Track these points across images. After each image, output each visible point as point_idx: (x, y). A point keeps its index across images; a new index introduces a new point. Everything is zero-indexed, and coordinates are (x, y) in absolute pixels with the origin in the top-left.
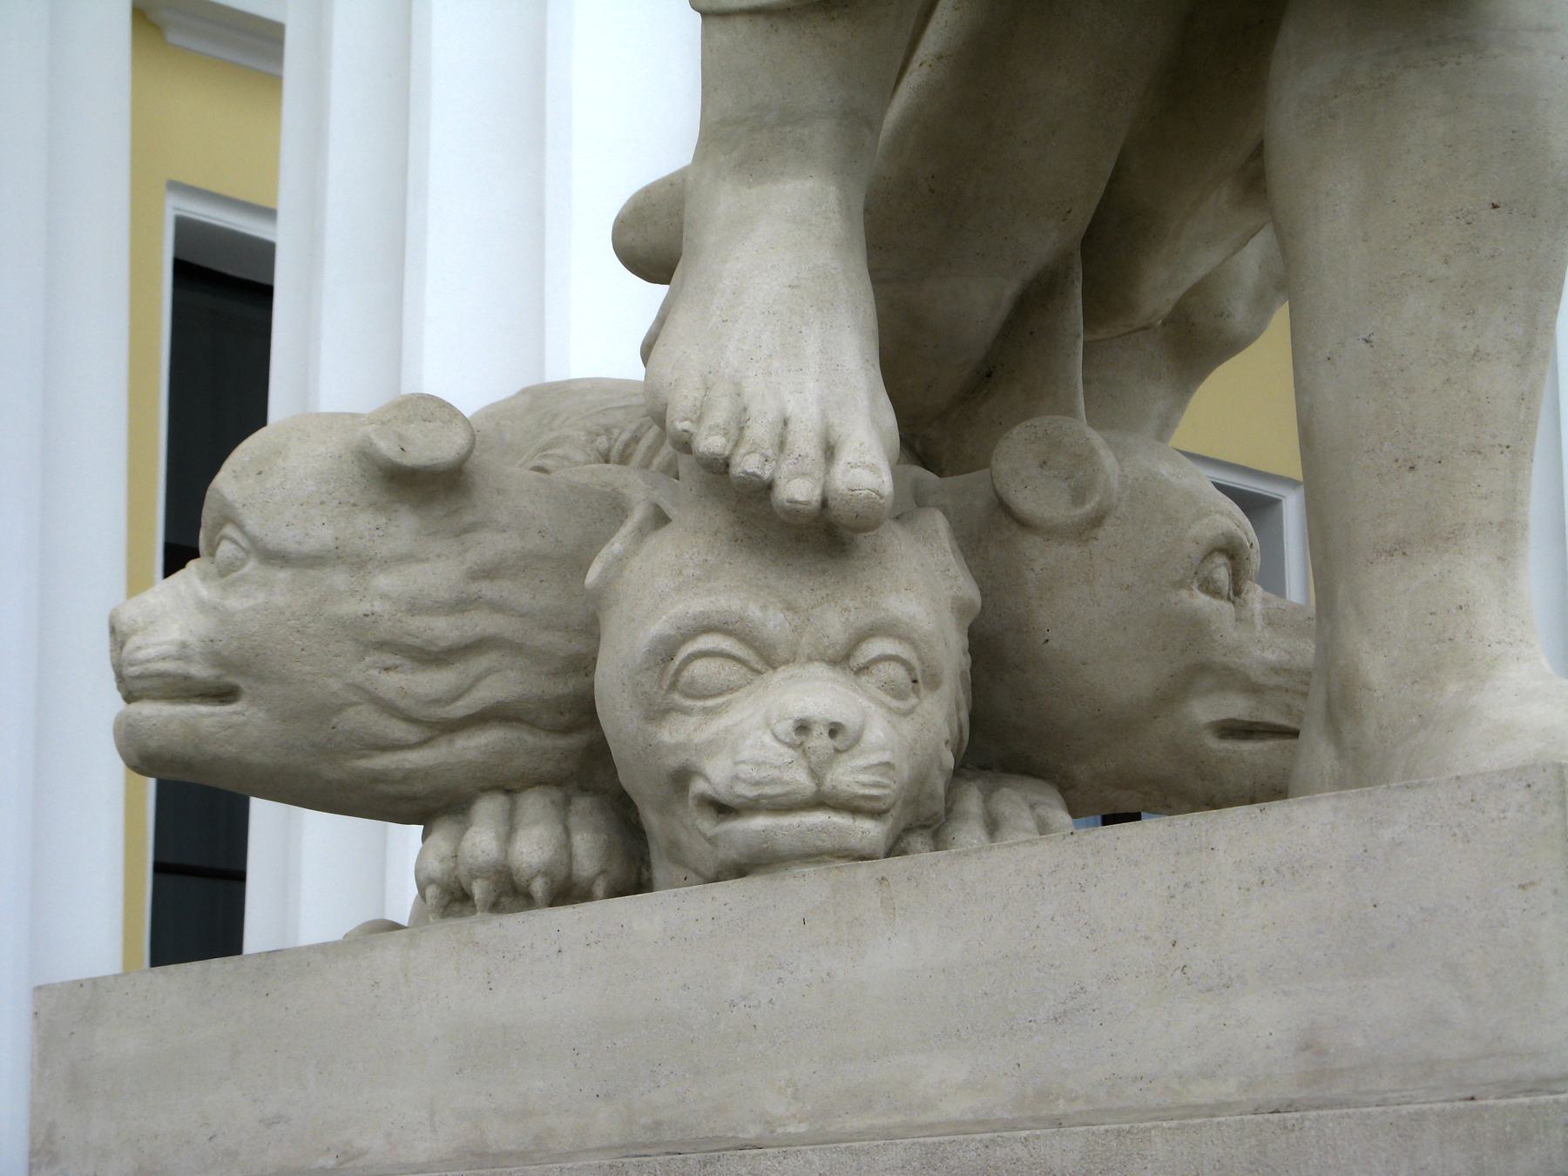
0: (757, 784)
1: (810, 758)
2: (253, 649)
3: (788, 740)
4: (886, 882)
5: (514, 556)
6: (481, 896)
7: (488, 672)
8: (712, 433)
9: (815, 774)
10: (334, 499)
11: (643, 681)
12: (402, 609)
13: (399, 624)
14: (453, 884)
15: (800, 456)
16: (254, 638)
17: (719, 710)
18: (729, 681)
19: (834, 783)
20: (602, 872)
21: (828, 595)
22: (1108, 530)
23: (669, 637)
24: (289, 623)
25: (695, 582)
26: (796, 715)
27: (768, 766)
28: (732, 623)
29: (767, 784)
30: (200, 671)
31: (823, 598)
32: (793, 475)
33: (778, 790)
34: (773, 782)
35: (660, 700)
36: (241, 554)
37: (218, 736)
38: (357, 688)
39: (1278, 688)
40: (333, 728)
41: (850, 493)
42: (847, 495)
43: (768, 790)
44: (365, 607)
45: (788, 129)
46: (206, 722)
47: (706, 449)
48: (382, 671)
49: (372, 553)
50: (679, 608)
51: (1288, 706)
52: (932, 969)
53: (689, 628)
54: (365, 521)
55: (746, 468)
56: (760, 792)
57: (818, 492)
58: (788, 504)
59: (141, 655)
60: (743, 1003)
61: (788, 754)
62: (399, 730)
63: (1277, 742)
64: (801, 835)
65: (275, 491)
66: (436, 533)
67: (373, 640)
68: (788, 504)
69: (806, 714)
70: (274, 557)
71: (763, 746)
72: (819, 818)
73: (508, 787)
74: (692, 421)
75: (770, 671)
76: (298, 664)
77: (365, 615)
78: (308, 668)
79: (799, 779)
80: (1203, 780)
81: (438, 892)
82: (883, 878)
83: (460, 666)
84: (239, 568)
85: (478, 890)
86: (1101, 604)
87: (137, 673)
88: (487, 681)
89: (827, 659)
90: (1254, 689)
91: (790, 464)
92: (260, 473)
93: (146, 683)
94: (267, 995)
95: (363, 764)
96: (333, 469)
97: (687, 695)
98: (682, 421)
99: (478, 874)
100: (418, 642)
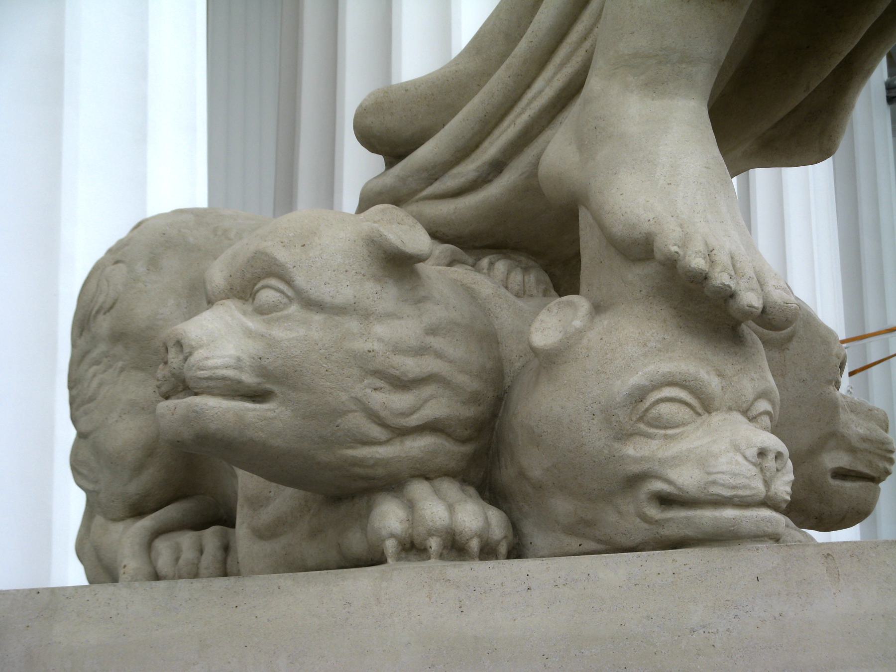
0: (734, 487)
1: (765, 473)
2: (293, 366)
3: (753, 461)
4: (831, 557)
5: (445, 321)
6: (436, 548)
7: (432, 397)
8: (697, 256)
9: (767, 483)
10: (353, 269)
11: (619, 414)
12: (390, 350)
13: (388, 360)
14: (407, 539)
15: (750, 277)
16: (295, 359)
17: (677, 437)
18: (684, 418)
19: (776, 491)
20: (505, 537)
21: (741, 369)
22: (794, 345)
23: (644, 386)
24: (321, 351)
25: (657, 352)
26: (759, 445)
27: (742, 477)
28: (689, 381)
29: (740, 488)
30: (249, 379)
31: (739, 370)
32: (747, 289)
33: (748, 492)
34: (745, 487)
35: (628, 427)
36: (285, 300)
37: (256, 424)
38: (357, 400)
39: (866, 450)
40: (337, 426)
41: (786, 305)
42: (784, 306)
43: (741, 492)
44: (368, 346)
45: (684, 66)
46: (251, 414)
47: (696, 266)
48: (373, 391)
49: (374, 309)
50: (651, 368)
51: (870, 462)
52: (873, 615)
53: (658, 381)
54: (370, 287)
55: (724, 281)
56: (735, 493)
57: (761, 302)
58: (747, 308)
59: (210, 363)
60: (703, 630)
61: (754, 470)
62: (376, 432)
63: (863, 483)
64: (757, 523)
65: (317, 259)
66: (406, 300)
67: (372, 369)
68: (747, 308)
69: (765, 445)
70: (312, 304)
71: (738, 463)
72: (766, 513)
73: (428, 476)
74: (679, 247)
75: (707, 414)
76: (322, 380)
77: (369, 351)
78: (328, 384)
79: (758, 487)
80: (820, 503)
81: (396, 543)
82: (828, 554)
83: (417, 392)
84: (281, 310)
85: (434, 544)
86: (789, 390)
87: (206, 376)
88: (430, 404)
89: (741, 410)
90: (852, 450)
91: (744, 281)
92: (304, 246)
93: (212, 384)
94: (236, 607)
95: (350, 452)
96: (351, 249)
97: (650, 425)
98: (673, 246)
99: (434, 533)
100: (397, 373)
